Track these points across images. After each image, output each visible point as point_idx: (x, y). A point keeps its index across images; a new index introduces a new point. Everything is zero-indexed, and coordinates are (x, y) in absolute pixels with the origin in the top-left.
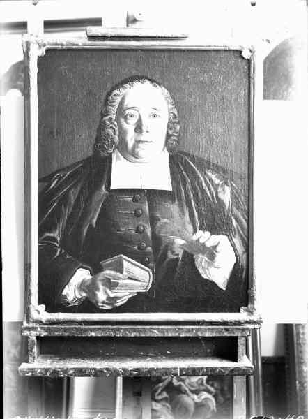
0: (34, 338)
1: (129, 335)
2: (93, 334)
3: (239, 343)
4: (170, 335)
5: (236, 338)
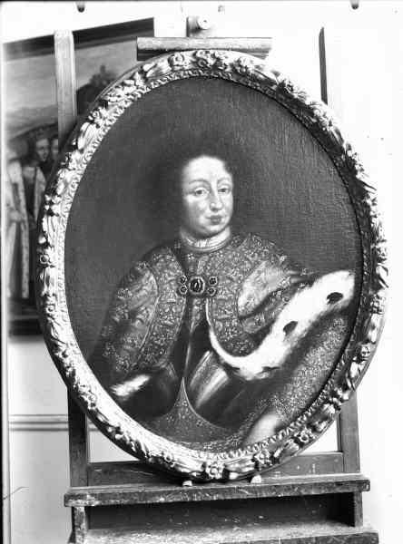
0: (83, 509)
1: (210, 498)
2: (162, 500)
3: (234, 541)
4: (264, 496)
5: (351, 495)
